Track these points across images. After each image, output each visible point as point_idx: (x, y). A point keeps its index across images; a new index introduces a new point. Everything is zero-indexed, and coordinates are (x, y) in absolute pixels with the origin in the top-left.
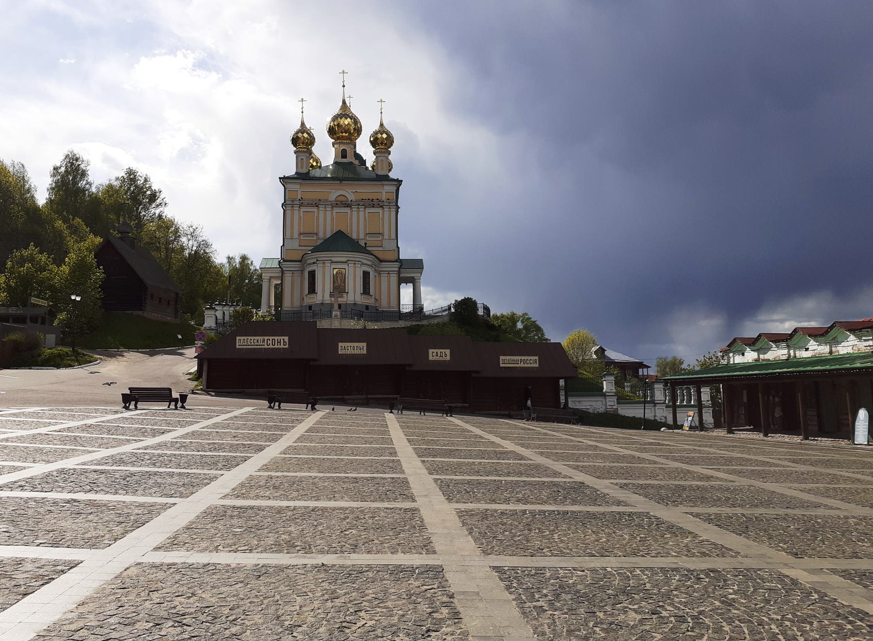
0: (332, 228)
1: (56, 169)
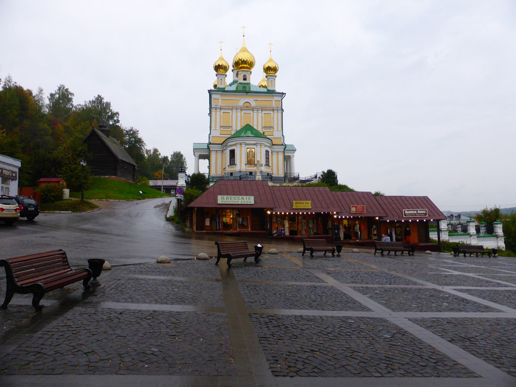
0: (241, 124)
1: (52, 95)
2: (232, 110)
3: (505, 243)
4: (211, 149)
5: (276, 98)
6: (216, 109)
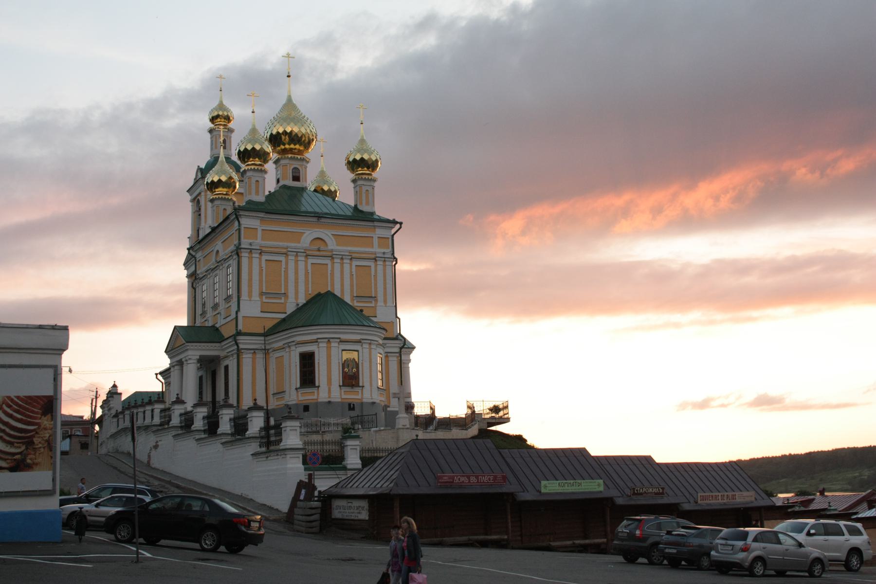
0: (307, 290)
4: (241, 346)
5: (380, 232)
6: (251, 251)
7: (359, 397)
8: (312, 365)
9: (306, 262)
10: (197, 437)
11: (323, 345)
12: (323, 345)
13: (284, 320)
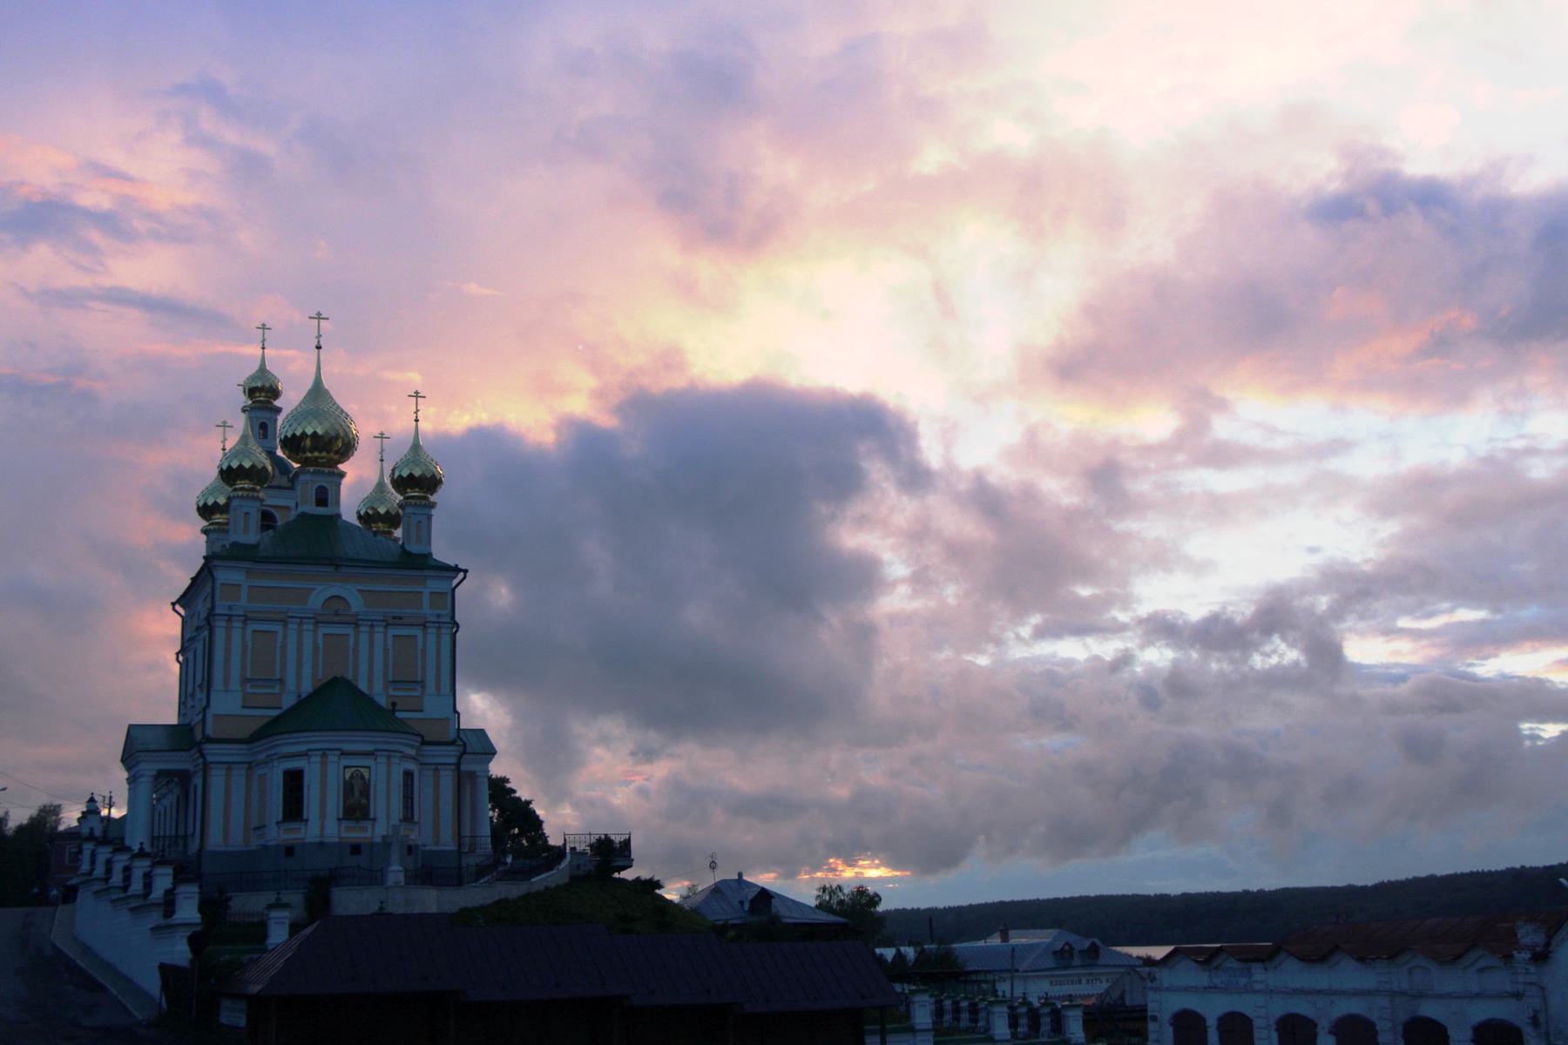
2: (284, 622)
3: (200, 910)
4: (210, 759)
5: (435, 585)
6: (230, 618)
7: (369, 834)
8: (300, 788)
9: (315, 632)
10: (114, 897)
11: (316, 759)
12: (316, 759)
13: (277, 719)
